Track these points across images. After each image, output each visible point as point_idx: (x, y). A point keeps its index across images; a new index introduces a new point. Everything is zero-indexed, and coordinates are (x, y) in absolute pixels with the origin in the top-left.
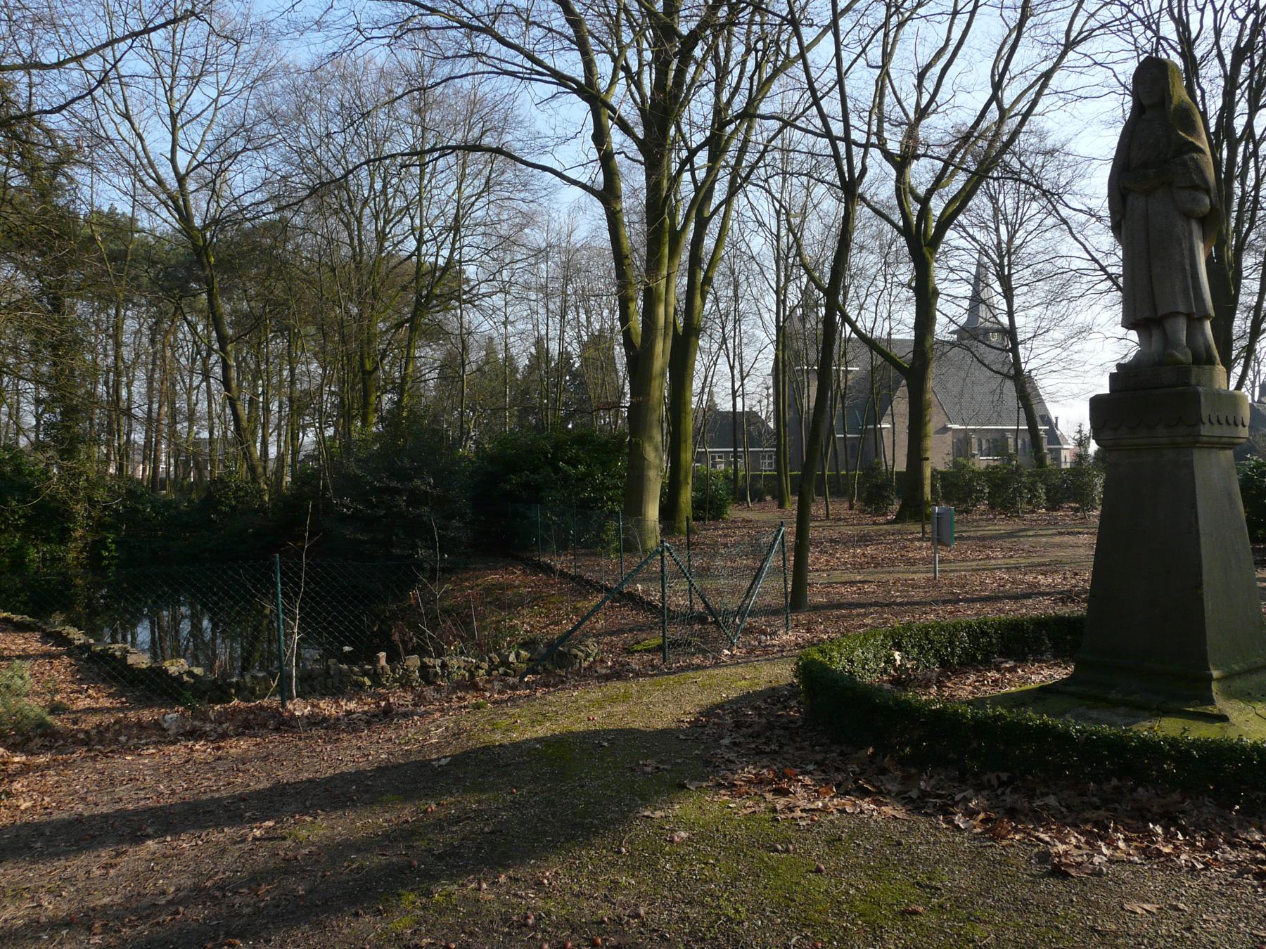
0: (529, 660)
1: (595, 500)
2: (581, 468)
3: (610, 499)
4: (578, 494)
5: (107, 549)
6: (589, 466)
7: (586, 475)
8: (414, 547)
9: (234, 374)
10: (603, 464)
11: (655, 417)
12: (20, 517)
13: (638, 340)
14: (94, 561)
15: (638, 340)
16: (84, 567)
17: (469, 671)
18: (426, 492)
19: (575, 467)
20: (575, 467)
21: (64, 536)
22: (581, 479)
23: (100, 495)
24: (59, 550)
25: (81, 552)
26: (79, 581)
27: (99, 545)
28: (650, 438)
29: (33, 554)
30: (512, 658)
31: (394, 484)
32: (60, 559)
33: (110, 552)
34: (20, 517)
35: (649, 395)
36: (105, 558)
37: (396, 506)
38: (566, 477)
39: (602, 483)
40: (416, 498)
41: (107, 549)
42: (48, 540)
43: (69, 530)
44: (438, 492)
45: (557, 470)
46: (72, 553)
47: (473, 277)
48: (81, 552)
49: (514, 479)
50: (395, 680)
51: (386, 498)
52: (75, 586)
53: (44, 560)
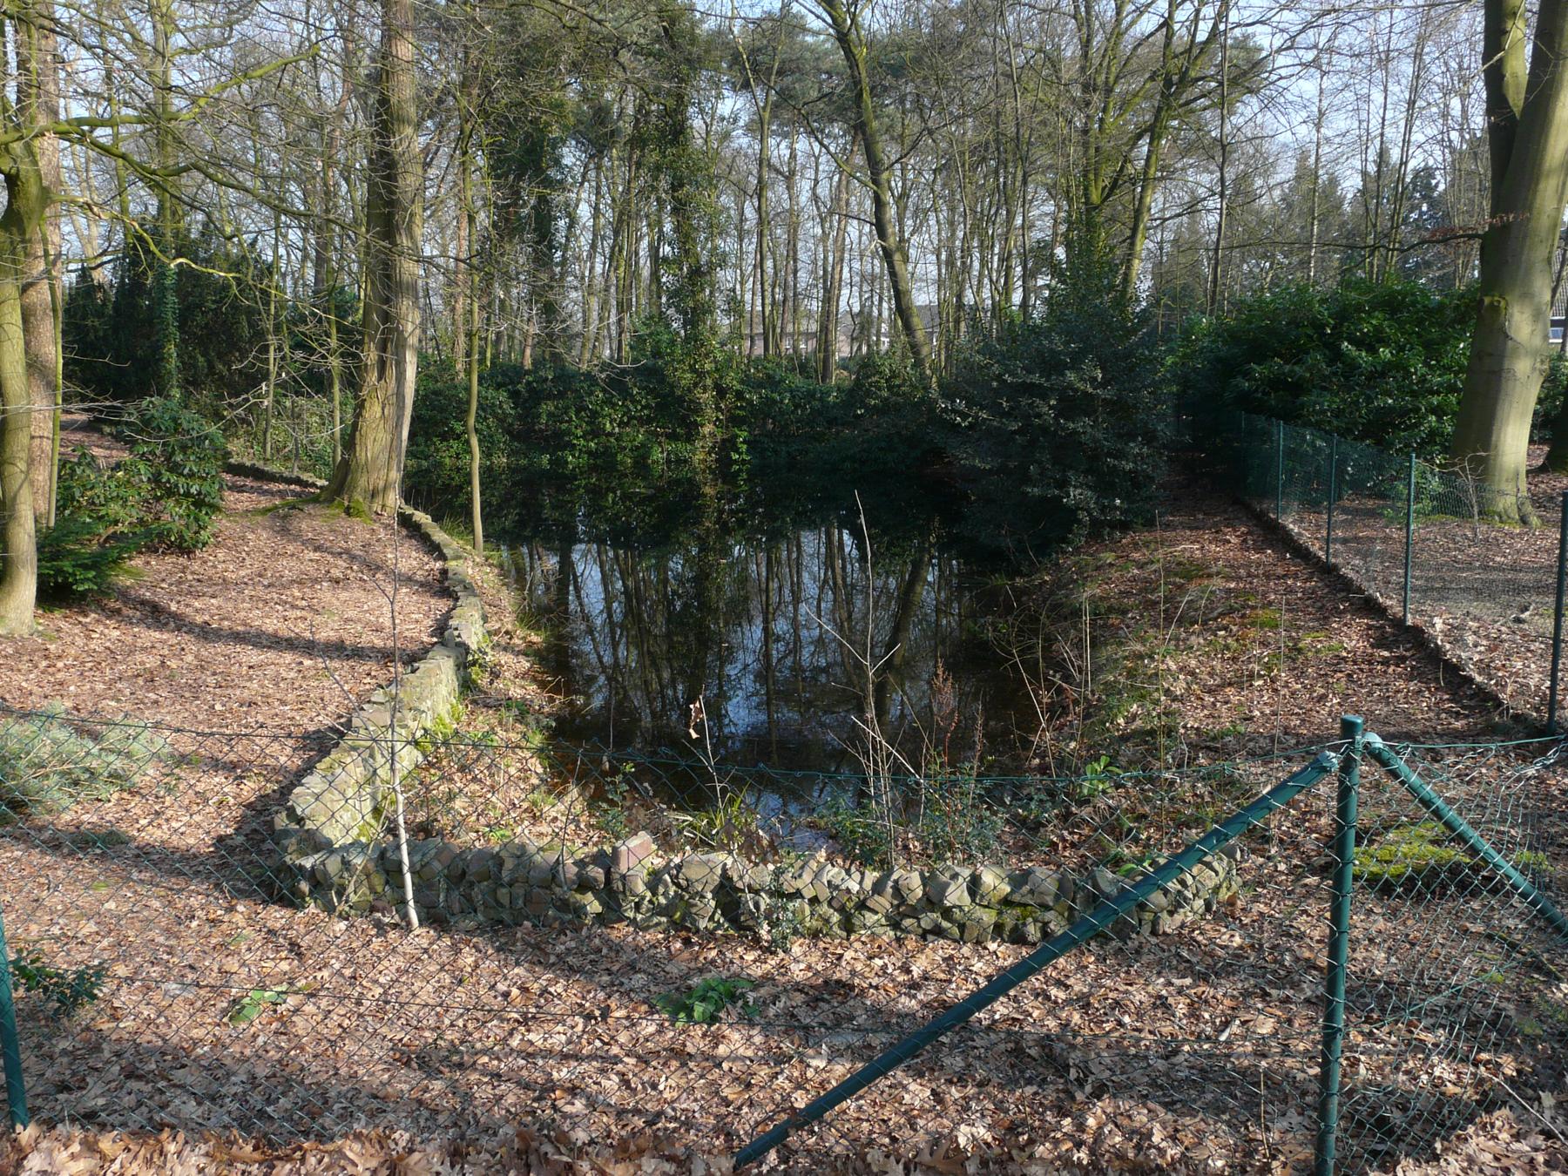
0: (1006, 902)
1: (1404, 413)
2: (1385, 353)
3: (1434, 410)
4: (1369, 400)
5: (737, 451)
6: (1401, 349)
7: (1388, 367)
8: (1063, 484)
9: (892, 211)
10: (1427, 345)
11: (1541, 253)
12: (644, 408)
13: (1516, 97)
14: (723, 469)
15: (1516, 97)
16: (712, 472)
17: (841, 910)
18: (1085, 393)
19: (1372, 350)
20: (1372, 350)
21: (690, 432)
22: (1380, 373)
23: (732, 380)
24: (682, 448)
25: (709, 453)
26: (708, 490)
27: (728, 445)
28: (1527, 295)
29: (657, 455)
30: (957, 895)
31: (1036, 378)
32: (686, 461)
33: (740, 454)
34: (644, 408)
35: (1530, 208)
36: (736, 462)
37: (1039, 416)
38: (1352, 367)
39: (1423, 380)
40: (1073, 404)
41: (737, 451)
42: (673, 437)
43: (696, 425)
44: (1107, 393)
45: (1336, 355)
46: (700, 455)
47: (1266, 44)
48: (709, 453)
49: (1258, 370)
50: (658, 910)
51: (1024, 401)
52: (705, 495)
53: (668, 461)
